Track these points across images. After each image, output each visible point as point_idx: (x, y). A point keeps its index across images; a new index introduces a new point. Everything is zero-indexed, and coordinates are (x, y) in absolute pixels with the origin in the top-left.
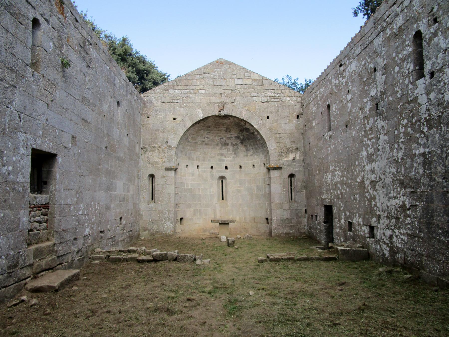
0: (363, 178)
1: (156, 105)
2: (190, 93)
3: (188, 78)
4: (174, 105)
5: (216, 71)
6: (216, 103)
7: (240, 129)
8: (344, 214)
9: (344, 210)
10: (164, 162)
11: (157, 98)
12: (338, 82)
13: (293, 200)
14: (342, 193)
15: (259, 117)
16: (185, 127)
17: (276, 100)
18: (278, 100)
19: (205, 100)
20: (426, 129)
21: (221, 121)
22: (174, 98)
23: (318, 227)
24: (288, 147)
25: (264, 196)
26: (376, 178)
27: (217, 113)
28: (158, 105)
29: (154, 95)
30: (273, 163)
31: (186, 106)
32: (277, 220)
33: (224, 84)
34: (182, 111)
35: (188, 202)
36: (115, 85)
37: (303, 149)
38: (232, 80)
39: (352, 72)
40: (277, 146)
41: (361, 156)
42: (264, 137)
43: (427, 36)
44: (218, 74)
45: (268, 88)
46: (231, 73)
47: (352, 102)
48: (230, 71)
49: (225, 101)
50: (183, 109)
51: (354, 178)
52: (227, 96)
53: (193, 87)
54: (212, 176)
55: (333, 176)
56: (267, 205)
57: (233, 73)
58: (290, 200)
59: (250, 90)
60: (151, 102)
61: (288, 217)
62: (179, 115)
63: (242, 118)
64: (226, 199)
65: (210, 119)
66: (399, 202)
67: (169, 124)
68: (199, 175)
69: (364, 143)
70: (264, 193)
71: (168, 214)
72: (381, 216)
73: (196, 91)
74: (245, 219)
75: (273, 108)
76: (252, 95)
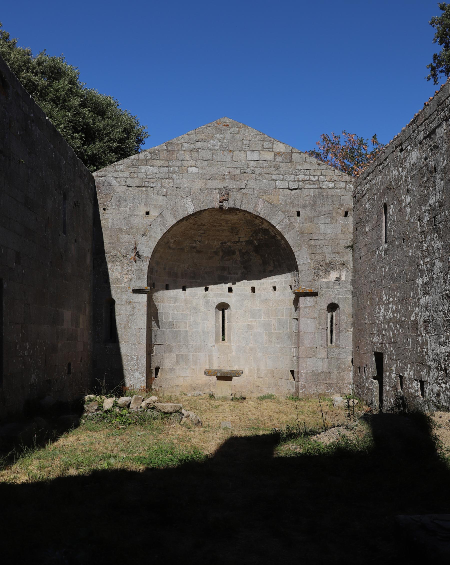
0: (417, 315)
1: (118, 190)
2: (173, 172)
3: (170, 148)
4: (146, 191)
5: (217, 137)
6: (216, 189)
8: (395, 365)
10: (131, 280)
11: (118, 180)
12: (397, 174)
13: (334, 343)
14: (394, 335)
15: (284, 212)
16: (165, 225)
17: (312, 186)
18: (316, 186)
19: (198, 184)
21: (223, 217)
22: (147, 180)
23: (367, 385)
24: (328, 261)
25: (290, 336)
26: (428, 317)
27: (216, 205)
28: (120, 189)
29: (114, 174)
30: (305, 287)
31: (167, 192)
32: (307, 373)
33: (229, 158)
34: (161, 200)
37: (352, 265)
38: (243, 152)
39: (413, 164)
40: (311, 259)
41: (416, 285)
42: (291, 244)
44: (219, 143)
45: (300, 167)
46: (240, 143)
47: (411, 207)
48: (239, 138)
49: (230, 187)
50: (161, 197)
51: (407, 315)
53: (179, 163)
54: (207, 303)
55: (386, 310)
56: (294, 350)
57: (245, 142)
58: (329, 344)
59: (272, 170)
60: (110, 185)
62: (155, 206)
64: (230, 340)
67: (139, 221)
68: (186, 300)
69: (420, 267)
70: (289, 332)
71: (137, 360)
72: (432, 367)
73: (183, 170)
74: (258, 371)
75: (307, 198)
76: (274, 177)
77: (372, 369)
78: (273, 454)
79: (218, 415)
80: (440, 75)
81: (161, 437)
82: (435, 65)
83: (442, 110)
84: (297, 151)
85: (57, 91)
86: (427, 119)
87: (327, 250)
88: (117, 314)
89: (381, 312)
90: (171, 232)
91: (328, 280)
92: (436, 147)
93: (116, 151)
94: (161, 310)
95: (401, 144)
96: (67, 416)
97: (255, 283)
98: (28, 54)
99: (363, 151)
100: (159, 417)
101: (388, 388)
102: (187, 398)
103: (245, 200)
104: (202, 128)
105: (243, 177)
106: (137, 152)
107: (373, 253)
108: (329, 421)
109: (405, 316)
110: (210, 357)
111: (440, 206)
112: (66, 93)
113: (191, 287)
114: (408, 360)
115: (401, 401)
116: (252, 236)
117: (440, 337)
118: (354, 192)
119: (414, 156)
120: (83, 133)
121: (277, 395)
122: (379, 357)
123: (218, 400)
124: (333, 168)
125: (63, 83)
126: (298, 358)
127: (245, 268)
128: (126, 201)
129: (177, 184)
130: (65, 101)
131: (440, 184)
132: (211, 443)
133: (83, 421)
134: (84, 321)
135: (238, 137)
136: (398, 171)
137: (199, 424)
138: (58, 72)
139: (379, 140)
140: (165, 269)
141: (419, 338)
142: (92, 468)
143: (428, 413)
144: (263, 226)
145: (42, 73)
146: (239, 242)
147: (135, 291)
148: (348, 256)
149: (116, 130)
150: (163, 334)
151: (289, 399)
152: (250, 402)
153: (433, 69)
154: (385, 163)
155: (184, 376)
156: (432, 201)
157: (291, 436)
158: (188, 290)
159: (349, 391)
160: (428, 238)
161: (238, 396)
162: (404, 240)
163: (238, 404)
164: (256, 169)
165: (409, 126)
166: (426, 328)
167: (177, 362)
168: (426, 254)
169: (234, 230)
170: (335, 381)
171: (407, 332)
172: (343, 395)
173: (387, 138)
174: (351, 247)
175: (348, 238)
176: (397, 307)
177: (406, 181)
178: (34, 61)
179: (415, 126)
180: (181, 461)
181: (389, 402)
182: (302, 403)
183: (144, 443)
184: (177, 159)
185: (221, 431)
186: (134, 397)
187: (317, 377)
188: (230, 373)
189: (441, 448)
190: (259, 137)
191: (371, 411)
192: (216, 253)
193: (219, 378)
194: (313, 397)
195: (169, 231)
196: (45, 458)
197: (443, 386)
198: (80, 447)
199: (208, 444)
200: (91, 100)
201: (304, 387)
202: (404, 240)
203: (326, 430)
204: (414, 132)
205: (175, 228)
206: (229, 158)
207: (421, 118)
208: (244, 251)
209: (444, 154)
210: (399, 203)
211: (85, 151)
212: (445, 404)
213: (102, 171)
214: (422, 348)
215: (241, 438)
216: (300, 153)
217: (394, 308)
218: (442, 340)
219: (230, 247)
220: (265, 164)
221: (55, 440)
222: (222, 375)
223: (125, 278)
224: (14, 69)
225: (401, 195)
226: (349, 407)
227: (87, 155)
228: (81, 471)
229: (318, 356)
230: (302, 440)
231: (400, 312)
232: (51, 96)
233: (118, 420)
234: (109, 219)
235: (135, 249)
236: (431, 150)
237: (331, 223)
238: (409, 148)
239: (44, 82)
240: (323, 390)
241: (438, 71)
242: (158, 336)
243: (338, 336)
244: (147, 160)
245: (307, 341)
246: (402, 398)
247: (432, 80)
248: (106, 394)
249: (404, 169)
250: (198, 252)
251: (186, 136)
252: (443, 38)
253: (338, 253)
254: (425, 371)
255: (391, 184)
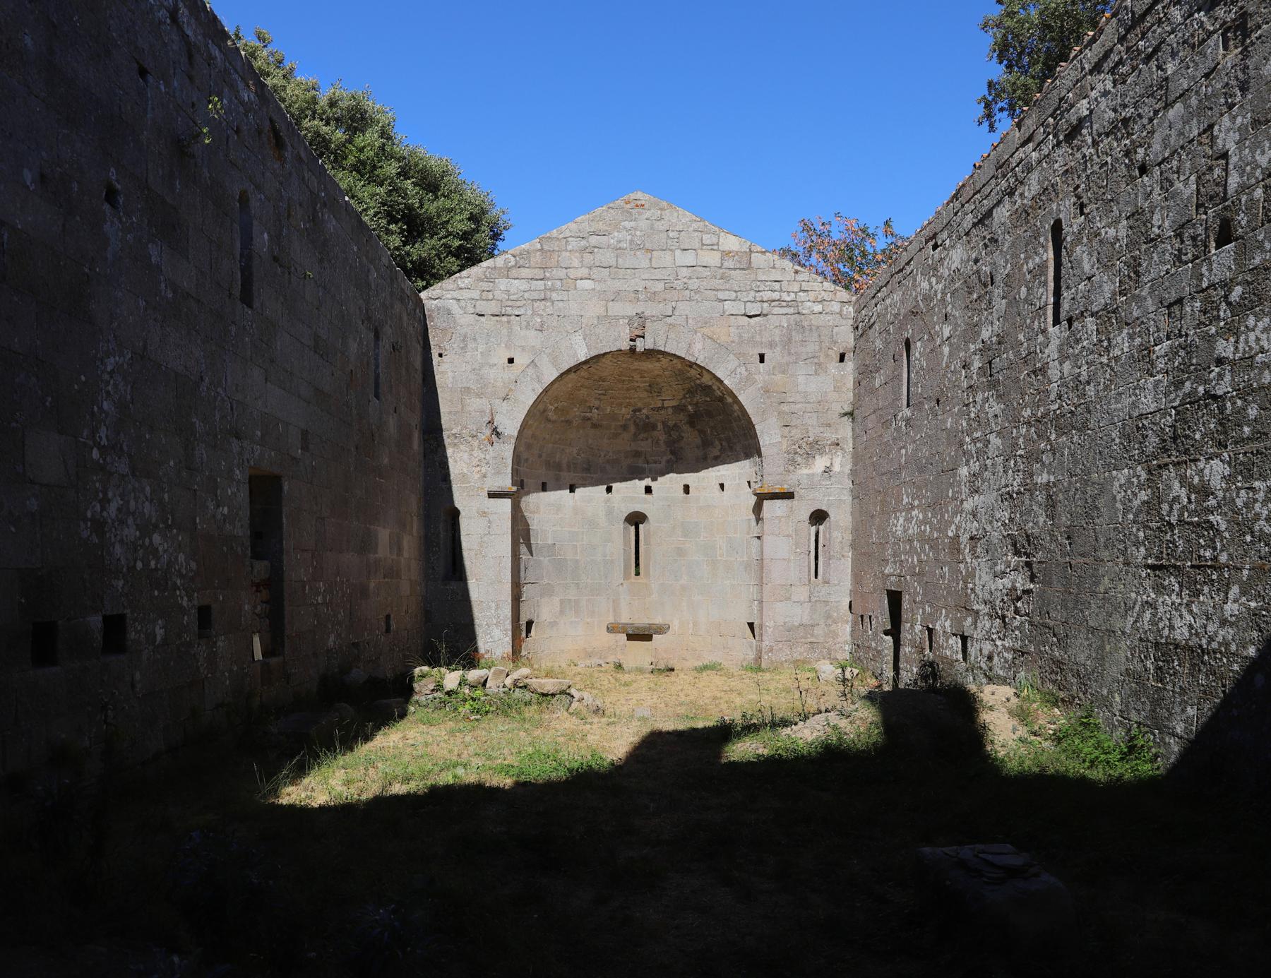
0: (958, 528)
2: (553, 289)
3: (546, 247)
6: (623, 317)
7: (687, 386)
9: (922, 602)
10: (485, 476)
14: (920, 561)
15: (738, 356)
18: (791, 310)
19: (595, 309)
20: (1053, 437)
21: (636, 365)
23: (874, 644)
26: (978, 530)
27: (625, 345)
28: (465, 321)
29: (456, 294)
30: (772, 485)
31: (542, 324)
33: (645, 264)
34: (533, 338)
35: (546, 581)
36: (369, 285)
38: (668, 253)
40: (783, 437)
42: (750, 411)
43: (1069, 239)
46: (664, 235)
47: (950, 345)
48: (661, 228)
52: (653, 297)
53: (561, 273)
54: (610, 512)
57: (671, 234)
59: (717, 283)
61: (805, 622)
63: (693, 360)
64: (648, 574)
65: (607, 361)
66: (1006, 582)
67: (498, 375)
71: (497, 609)
75: (777, 331)
76: (721, 295)
77: (883, 620)
78: (721, 758)
79: (630, 696)
80: (999, 115)
81: (537, 733)
82: (990, 98)
83: (1004, 176)
84: (759, 249)
85: (361, 150)
86: (979, 192)
87: (811, 420)
88: (463, 533)
89: (899, 524)
90: (550, 392)
91: (810, 472)
92: (994, 240)
93: (457, 253)
94: (534, 525)
95: (934, 236)
96: (384, 701)
97: (689, 478)
98: (314, 88)
99: (869, 249)
100: (534, 701)
101: (907, 649)
102: (579, 669)
103: (672, 335)
104: (599, 211)
105: (668, 296)
106: (491, 255)
107: (886, 424)
108: (812, 704)
109: (939, 530)
110: (616, 603)
111: (999, 343)
112: (377, 155)
113: (584, 486)
114: (942, 602)
115: (930, 670)
116: (684, 397)
117: (996, 564)
118: (855, 318)
119: (957, 256)
120: (406, 223)
121: (725, 664)
122: (895, 599)
123: (629, 672)
124: (820, 278)
125: (370, 137)
126: (761, 602)
127: (672, 453)
128: (475, 340)
129: (560, 310)
130: (374, 168)
131: (1000, 305)
132: (619, 742)
133: (412, 709)
134: (410, 544)
135: (660, 226)
136: (930, 283)
137: (598, 711)
138: (363, 118)
139: (897, 228)
140: (540, 456)
141: (962, 566)
142: (429, 783)
143: (972, 687)
144: (703, 380)
145: (337, 120)
146: (662, 408)
147: (493, 495)
148: (845, 430)
149: (458, 217)
150: (539, 567)
151: (746, 669)
152: (682, 675)
153: (988, 106)
154: (908, 270)
155: (570, 638)
156: (985, 334)
157: (750, 729)
158: (579, 491)
159: (844, 654)
160: (979, 398)
161: (662, 667)
162: (938, 401)
163: (662, 679)
164: (690, 282)
165: (948, 204)
166: (973, 550)
167: (562, 612)
168: (975, 425)
169: (654, 388)
170: (821, 640)
171: (942, 557)
172: (833, 660)
173: (910, 226)
174: (851, 414)
175: (845, 400)
176: (925, 515)
177: (943, 299)
178: (323, 102)
179: (957, 204)
180: (571, 770)
181: (909, 674)
182: (767, 676)
183: (510, 742)
184: (558, 266)
185: (635, 723)
186: (493, 670)
187: (791, 633)
188: (649, 629)
189: (992, 742)
190: (695, 225)
191: (880, 686)
192: (625, 427)
193: (631, 637)
194: (786, 665)
195: (546, 391)
196: (354, 767)
197: (999, 643)
198: (408, 750)
199: (615, 744)
200: (416, 165)
201: (771, 650)
202: (938, 401)
203: (806, 718)
204: (956, 214)
205: (556, 386)
206: (645, 264)
207: (969, 191)
208: (671, 423)
209: (1007, 253)
210: (932, 338)
211: (408, 254)
212: (1001, 673)
213: (435, 290)
214: (965, 582)
215: (668, 733)
216: (763, 253)
217: (921, 516)
218: (998, 568)
219: (647, 417)
220: (706, 273)
221: (368, 738)
222: (637, 632)
223: (476, 471)
224: (292, 115)
225: (935, 324)
226: (844, 680)
227: (411, 262)
228: (412, 787)
229: (794, 598)
230: (766, 734)
231: (931, 524)
232: (352, 159)
233: (467, 706)
234: (447, 373)
235: (491, 422)
236: (986, 246)
237: (816, 373)
238: (947, 242)
239: (340, 135)
240: (801, 654)
241: (996, 108)
242: (530, 569)
243: (827, 565)
244: (509, 269)
245: (776, 574)
246: (931, 664)
247: (986, 124)
248: (448, 665)
249: (939, 279)
250: (595, 426)
251: (572, 226)
252: (1002, 51)
253: (829, 425)
254: (970, 619)
255: (917, 306)
